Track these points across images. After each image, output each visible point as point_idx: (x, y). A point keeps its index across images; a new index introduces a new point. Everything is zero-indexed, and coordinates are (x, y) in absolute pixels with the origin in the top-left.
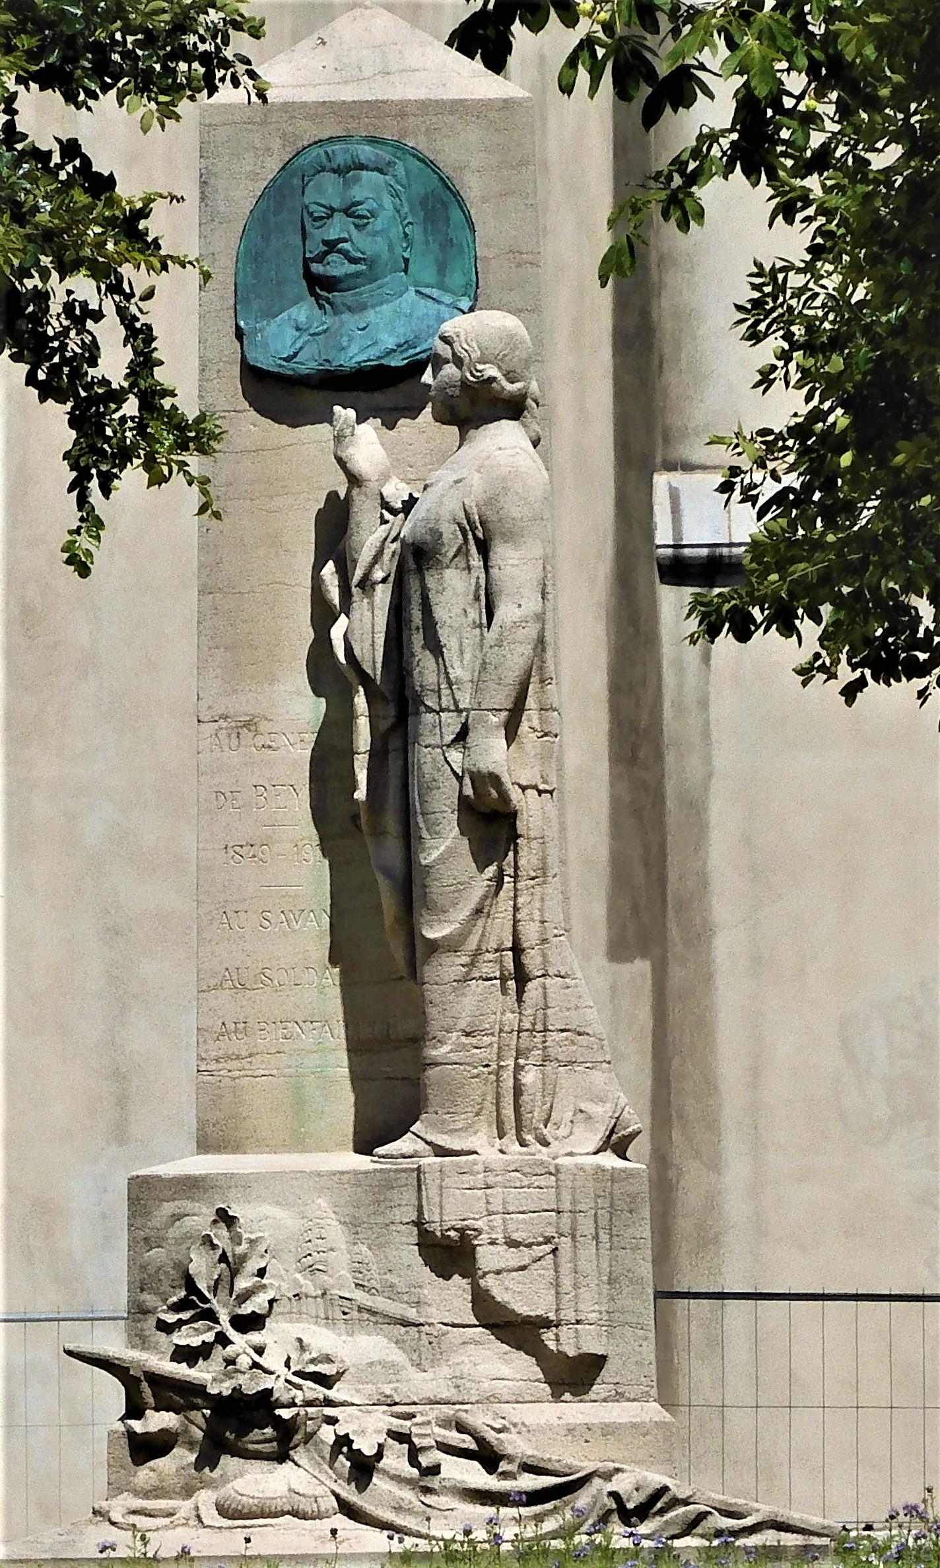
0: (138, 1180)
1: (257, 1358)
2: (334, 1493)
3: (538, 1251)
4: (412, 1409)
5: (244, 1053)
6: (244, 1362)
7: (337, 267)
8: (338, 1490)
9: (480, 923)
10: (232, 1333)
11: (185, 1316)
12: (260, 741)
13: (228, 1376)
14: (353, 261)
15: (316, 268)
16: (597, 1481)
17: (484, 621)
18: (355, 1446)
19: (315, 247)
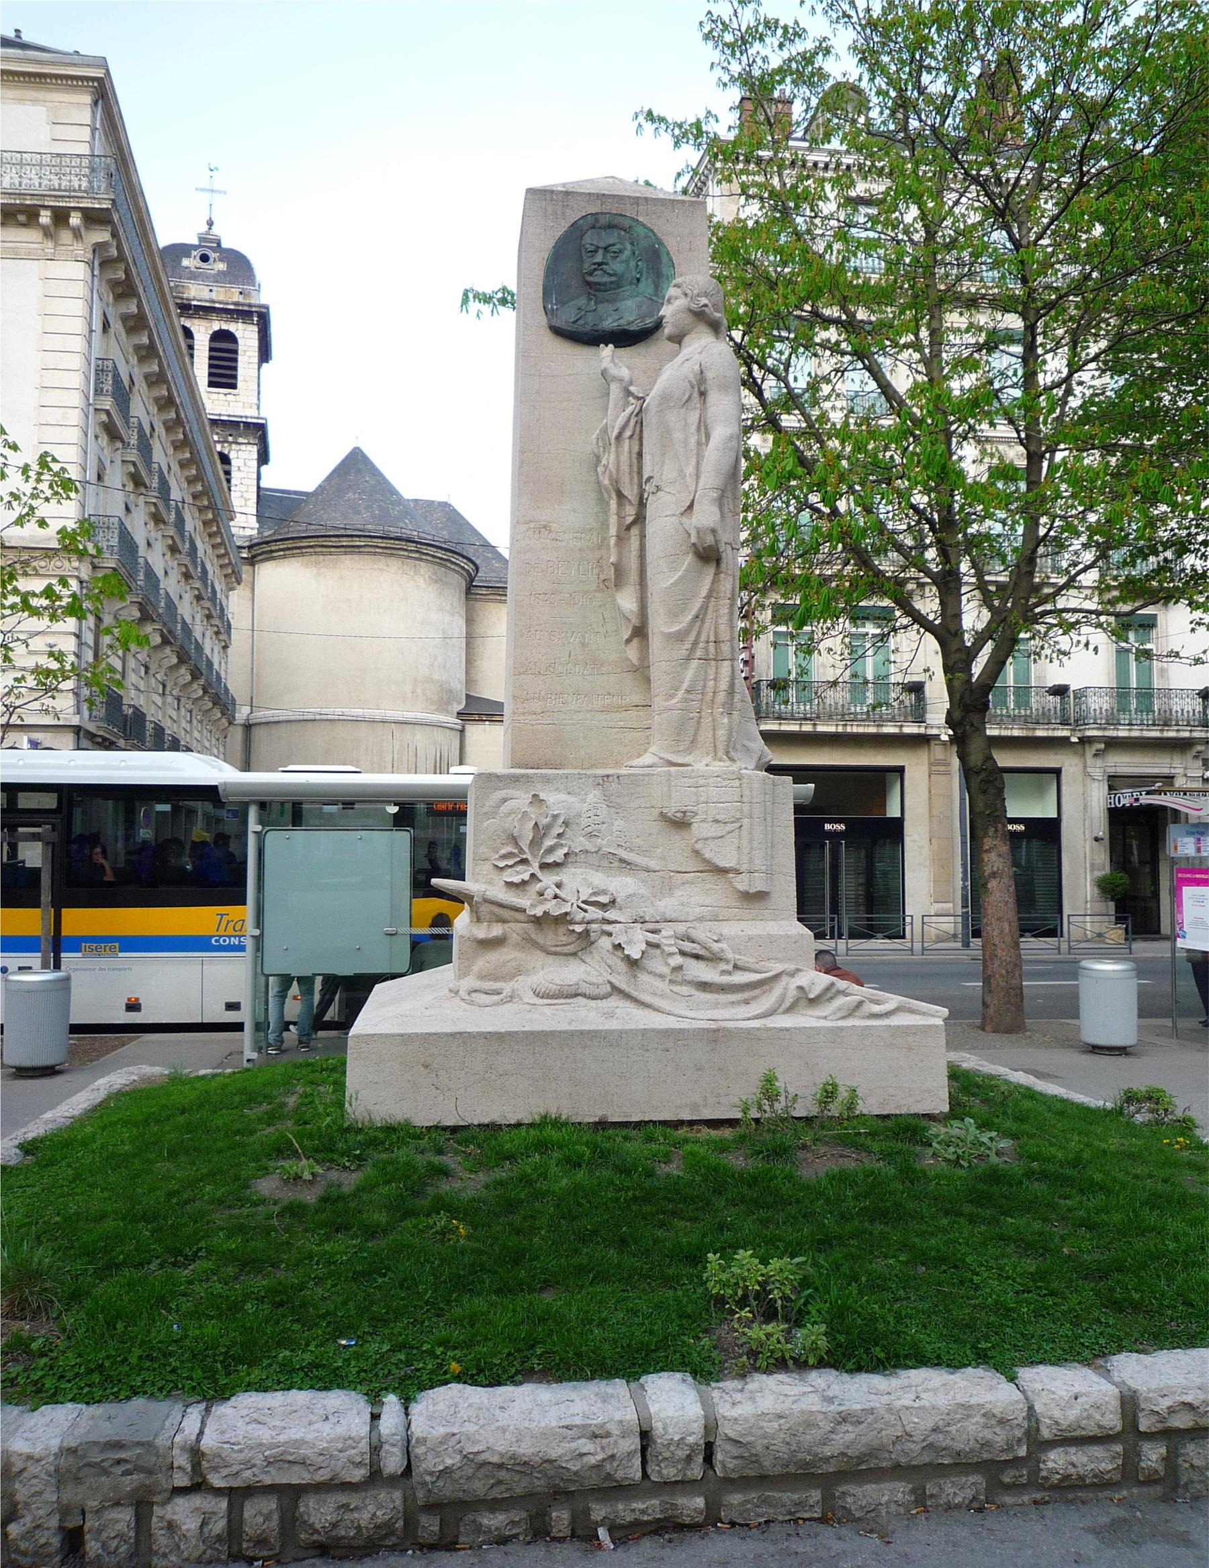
0: (889, 1123)
1: (558, 891)
2: (609, 982)
3: (730, 827)
4: (657, 926)
5: (539, 711)
6: (549, 893)
7: (598, 278)
8: (613, 980)
9: (698, 624)
10: (539, 875)
11: (510, 862)
12: (553, 536)
13: (541, 903)
14: (610, 275)
15: (591, 279)
16: (785, 979)
17: (704, 440)
18: (626, 952)
19: (587, 267)
